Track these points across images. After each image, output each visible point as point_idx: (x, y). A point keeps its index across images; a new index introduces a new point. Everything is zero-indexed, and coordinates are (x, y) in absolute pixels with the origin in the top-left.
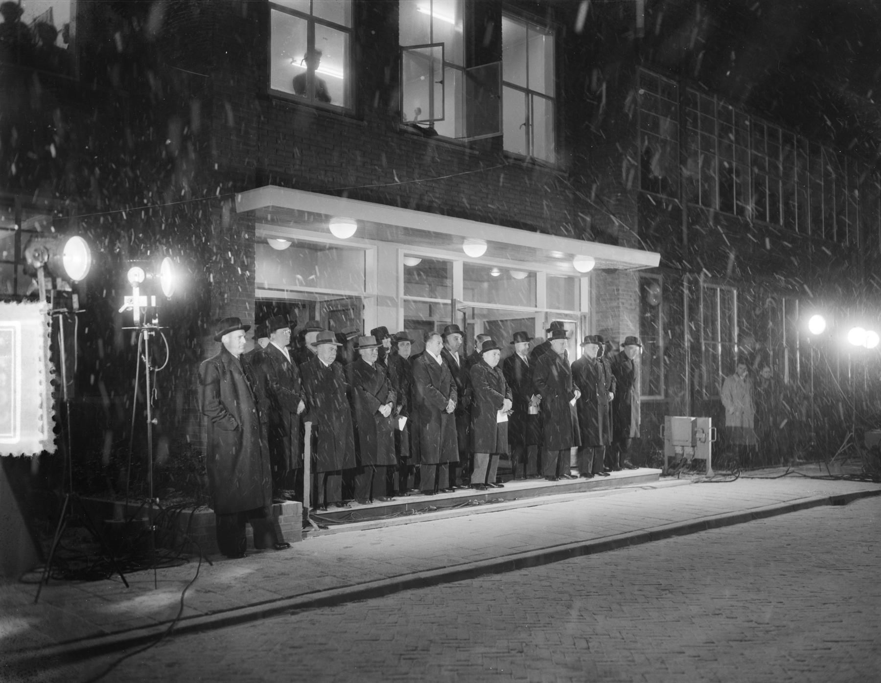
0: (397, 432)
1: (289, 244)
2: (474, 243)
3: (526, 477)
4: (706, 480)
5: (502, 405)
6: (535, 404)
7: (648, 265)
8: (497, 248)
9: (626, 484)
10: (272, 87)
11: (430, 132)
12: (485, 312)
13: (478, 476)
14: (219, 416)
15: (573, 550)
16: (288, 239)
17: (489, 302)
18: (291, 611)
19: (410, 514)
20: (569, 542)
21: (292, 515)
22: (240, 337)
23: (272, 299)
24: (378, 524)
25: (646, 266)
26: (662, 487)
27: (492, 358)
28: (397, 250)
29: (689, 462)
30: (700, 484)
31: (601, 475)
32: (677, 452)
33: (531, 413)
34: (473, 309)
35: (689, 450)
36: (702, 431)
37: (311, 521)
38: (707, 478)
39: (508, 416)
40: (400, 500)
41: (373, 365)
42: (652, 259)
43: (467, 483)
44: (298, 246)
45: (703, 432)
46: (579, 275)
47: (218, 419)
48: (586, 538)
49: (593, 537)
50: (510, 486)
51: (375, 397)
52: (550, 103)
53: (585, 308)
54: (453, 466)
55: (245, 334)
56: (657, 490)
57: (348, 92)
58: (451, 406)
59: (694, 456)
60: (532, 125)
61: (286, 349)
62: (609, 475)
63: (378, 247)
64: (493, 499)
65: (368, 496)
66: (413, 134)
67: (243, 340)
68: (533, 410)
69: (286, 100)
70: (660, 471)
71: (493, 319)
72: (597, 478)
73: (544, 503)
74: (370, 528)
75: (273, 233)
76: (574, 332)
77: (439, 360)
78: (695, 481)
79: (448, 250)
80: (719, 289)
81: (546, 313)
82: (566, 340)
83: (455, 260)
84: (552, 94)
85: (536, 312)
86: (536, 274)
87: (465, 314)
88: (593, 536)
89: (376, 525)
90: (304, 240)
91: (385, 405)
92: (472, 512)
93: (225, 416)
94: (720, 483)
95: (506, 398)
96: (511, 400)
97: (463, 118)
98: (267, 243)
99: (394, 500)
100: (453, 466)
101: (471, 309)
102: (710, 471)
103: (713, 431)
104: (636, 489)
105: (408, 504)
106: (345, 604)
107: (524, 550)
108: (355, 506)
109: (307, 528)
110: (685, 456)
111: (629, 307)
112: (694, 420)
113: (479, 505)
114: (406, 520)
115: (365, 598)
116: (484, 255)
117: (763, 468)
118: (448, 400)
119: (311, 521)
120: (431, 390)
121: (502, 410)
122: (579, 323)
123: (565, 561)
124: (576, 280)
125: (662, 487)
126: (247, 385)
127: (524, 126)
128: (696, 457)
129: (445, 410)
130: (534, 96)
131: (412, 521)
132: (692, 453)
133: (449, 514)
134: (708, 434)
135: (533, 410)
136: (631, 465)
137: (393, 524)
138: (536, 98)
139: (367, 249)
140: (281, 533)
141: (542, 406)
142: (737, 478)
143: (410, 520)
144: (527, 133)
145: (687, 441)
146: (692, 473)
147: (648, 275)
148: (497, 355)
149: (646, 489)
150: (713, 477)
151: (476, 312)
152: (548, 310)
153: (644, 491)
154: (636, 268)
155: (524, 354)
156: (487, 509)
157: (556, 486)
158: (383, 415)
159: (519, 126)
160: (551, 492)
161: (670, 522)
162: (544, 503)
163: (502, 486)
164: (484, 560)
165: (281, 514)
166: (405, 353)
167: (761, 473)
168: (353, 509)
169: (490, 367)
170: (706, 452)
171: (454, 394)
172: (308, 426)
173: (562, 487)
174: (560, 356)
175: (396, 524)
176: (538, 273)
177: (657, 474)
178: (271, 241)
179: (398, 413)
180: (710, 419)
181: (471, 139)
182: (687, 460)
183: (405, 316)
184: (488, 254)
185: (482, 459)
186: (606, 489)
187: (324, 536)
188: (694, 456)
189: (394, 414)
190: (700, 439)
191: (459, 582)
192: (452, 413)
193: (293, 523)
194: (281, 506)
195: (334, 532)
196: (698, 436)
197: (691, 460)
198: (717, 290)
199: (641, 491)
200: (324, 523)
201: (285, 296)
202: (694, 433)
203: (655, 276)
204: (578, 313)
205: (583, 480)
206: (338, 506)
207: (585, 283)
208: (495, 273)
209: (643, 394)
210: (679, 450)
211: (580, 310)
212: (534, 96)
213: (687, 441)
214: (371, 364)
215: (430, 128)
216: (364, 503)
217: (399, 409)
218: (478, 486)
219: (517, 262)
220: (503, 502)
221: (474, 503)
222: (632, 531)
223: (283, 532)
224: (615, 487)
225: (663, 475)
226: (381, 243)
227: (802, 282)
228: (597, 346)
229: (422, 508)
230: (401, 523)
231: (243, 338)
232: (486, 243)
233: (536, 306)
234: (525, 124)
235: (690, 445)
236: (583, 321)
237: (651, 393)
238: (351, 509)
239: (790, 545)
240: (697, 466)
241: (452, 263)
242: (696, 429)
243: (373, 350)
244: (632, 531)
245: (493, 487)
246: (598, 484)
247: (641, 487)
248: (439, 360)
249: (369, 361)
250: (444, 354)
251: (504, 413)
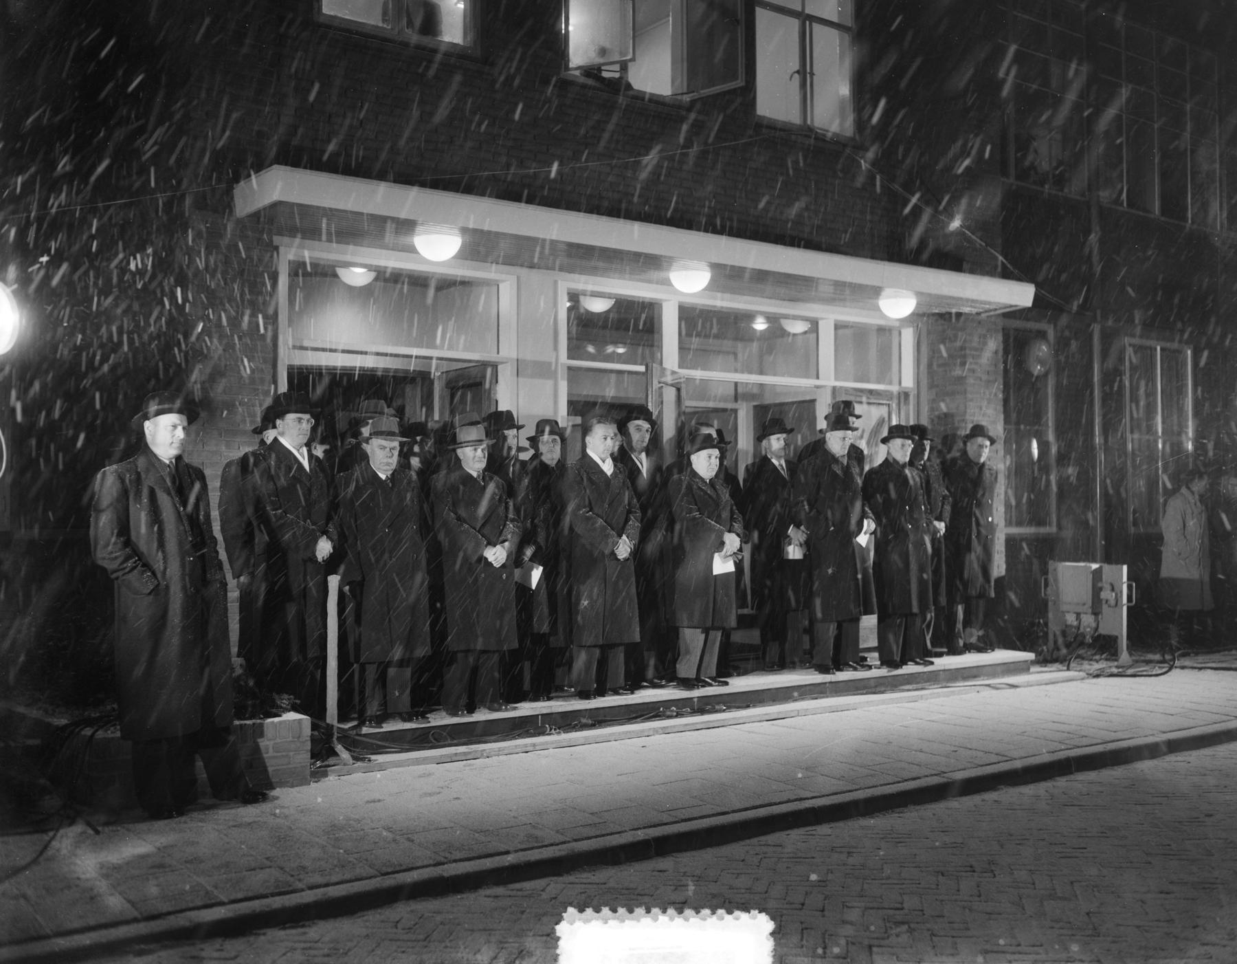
0: (523, 589)
1: (373, 275)
2: (686, 268)
3: (781, 665)
4: (1115, 671)
5: (723, 543)
6: (797, 542)
7: (1013, 303)
8: (727, 277)
9: (965, 678)
10: (325, 10)
11: (619, 86)
12: (755, 391)
13: (686, 668)
14: (124, 569)
15: (812, 811)
16: (369, 268)
17: (761, 373)
18: (137, 947)
19: (543, 733)
20: (785, 799)
21: (291, 739)
22: (175, 427)
23: (353, 369)
24: (470, 753)
25: (1011, 306)
26: (1029, 685)
27: (705, 463)
28: (556, 282)
29: (1089, 640)
30: (1102, 680)
31: (917, 663)
32: (1069, 623)
33: (791, 557)
34: (736, 384)
35: (1088, 620)
36: (1109, 587)
37: (339, 748)
38: (1117, 667)
39: (735, 562)
40: (526, 709)
41: (479, 476)
42: (1021, 295)
43: (668, 676)
44: (388, 279)
45: (1113, 590)
46: (897, 324)
47: (120, 573)
48: (823, 792)
49: (834, 789)
50: (740, 684)
51: (479, 532)
52: (847, 37)
53: (908, 381)
54: (633, 651)
55: (185, 424)
56: (1018, 689)
57: (468, 19)
58: (624, 549)
59: (1096, 629)
60: (812, 74)
61: (609, 462)
62: (932, 663)
63: (518, 278)
64: (704, 706)
65: (464, 701)
66: (594, 88)
67: (180, 433)
68: (794, 552)
69: (385, 40)
70: (1031, 656)
71: (768, 400)
72: (910, 669)
73: (799, 713)
74: (454, 759)
75: (348, 258)
76: (887, 419)
77: (608, 467)
78: (1095, 673)
79: (650, 281)
80: (1159, 348)
81: (834, 388)
82: (850, 432)
83: (666, 300)
84: (849, 22)
85: (817, 387)
86: (817, 323)
87: (679, 390)
88: (842, 786)
89: (465, 754)
90: (411, 271)
91: (495, 546)
93: (133, 568)
94: (1137, 679)
95: (730, 531)
96: (738, 535)
97: (682, 61)
98: (335, 276)
99: (515, 709)
100: (633, 651)
101: (733, 385)
102: (1125, 656)
103: (1130, 587)
104: (978, 688)
105: (542, 715)
106: (262, 931)
107: (687, 816)
108: (440, 719)
109: (330, 759)
110: (1082, 630)
111: (984, 377)
112: (1096, 570)
113: (676, 716)
114: (526, 746)
115: (308, 920)
116: (705, 289)
117: (1230, 650)
118: (620, 536)
119: (339, 748)
120: (588, 519)
121: (723, 553)
122: (894, 405)
123: (763, 839)
124: (895, 333)
125: (1029, 685)
126: (179, 512)
127: (796, 75)
128: (1102, 631)
129: (613, 554)
130: (814, 25)
131: (537, 748)
132: (1094, 625)
133: (610, 735)
134: (1121, 592)
135: (794, 552)
136: (982, 645)
137: (499, 752)
138: (817, 28)
139: (584, 293)
140: (266, 770)
141: (808, 545)
142: (1170, 669)
143: (534, 745)
144: (803, 85)
145: (1084, 604)
146: (1097, 657)
147: (1018, 324)
148: (713, 458)
149: (997, 689)
150: (1130, 667)
151: (740, 390)
152: (838, 384)
153: (994, 692)
154: (996, 310)
155: (779, 458)
156: (686, 725)
157: (831, 683)
158: (491, 564)
159: (788, 77)
160: (822, 693)
161: (1000, 758)
162: (799, 713)
163: (726, 684)
164: (596, 837)
165: (262, 735)
166: (549, 456)
167: (1223, 658)
168: (433, 724)
169: (702, 480)
170: (1118, 624)
171: (634, 524)
172: (334, 581)
173: (808, 688)
174: (840, 459)
175: (506, 752)
176: (820, 323)
177: (1026, 661)
178: (341, 272)
179: (526, 559)
180: (1125, 568)
181: (695, 95)
182: (1084, 637)
183: (569, 395)
184: (713, 286)
185: (692, 638)
186: (922, 689)
187: (360, 774)
188: (1096, 629)
189: (516, 560)
190: (1107, 601)
191: (518, 886)
192: (626, 560)
193: (291, 754)
194: (261, 725)
195: (381, 768)
196: (1103, 595)
197: (1092, 637)
198: (1156, 349)
199: (987, 693)
200: (362, 749)
201: (369, 362)
202: (1097, 591)
203: (1032, 325)
204: (894, 389)
205: (884, 672)
206: (405, 720)
207: (908, 337)
208: (760, 325)
209: (1009, 523)
210: (1071, 619)
211: (900, 383)
212: (814, 25)
213: (1084, 604)
214: (475, 474)
215: (621, 78)
216: (455, 714)
217: (529, 552)
218: (687, 684)
219: (786, 303)
220: (724, 711)
221: (668, 713)
222: (919, 778)
223: (270, 769)
224: (944, 684)
225: (1035, 662)
226: (524, 272)
227: (729, 112)
228: (910, 442)
229: (567, 722)
230: (517, 751)
231: (180, 428)
232: (708, 268)
233: (818, 378)
234: (798, 72)
235: (1090, 611)
236: (902, 400)
237: (1040, 523)
238: (428, 725)
239: (1210, 816)
240: (1105, 646)
241: (661, 306)
242: (1100, 585)
243: (475, 450)
244: (919, 778)
245: (711, 685)
246: (911, 679)
247: (988, 685)
248: (608, 467)
249: (471, 469)
250: (622, 457)
251: (726, 557)
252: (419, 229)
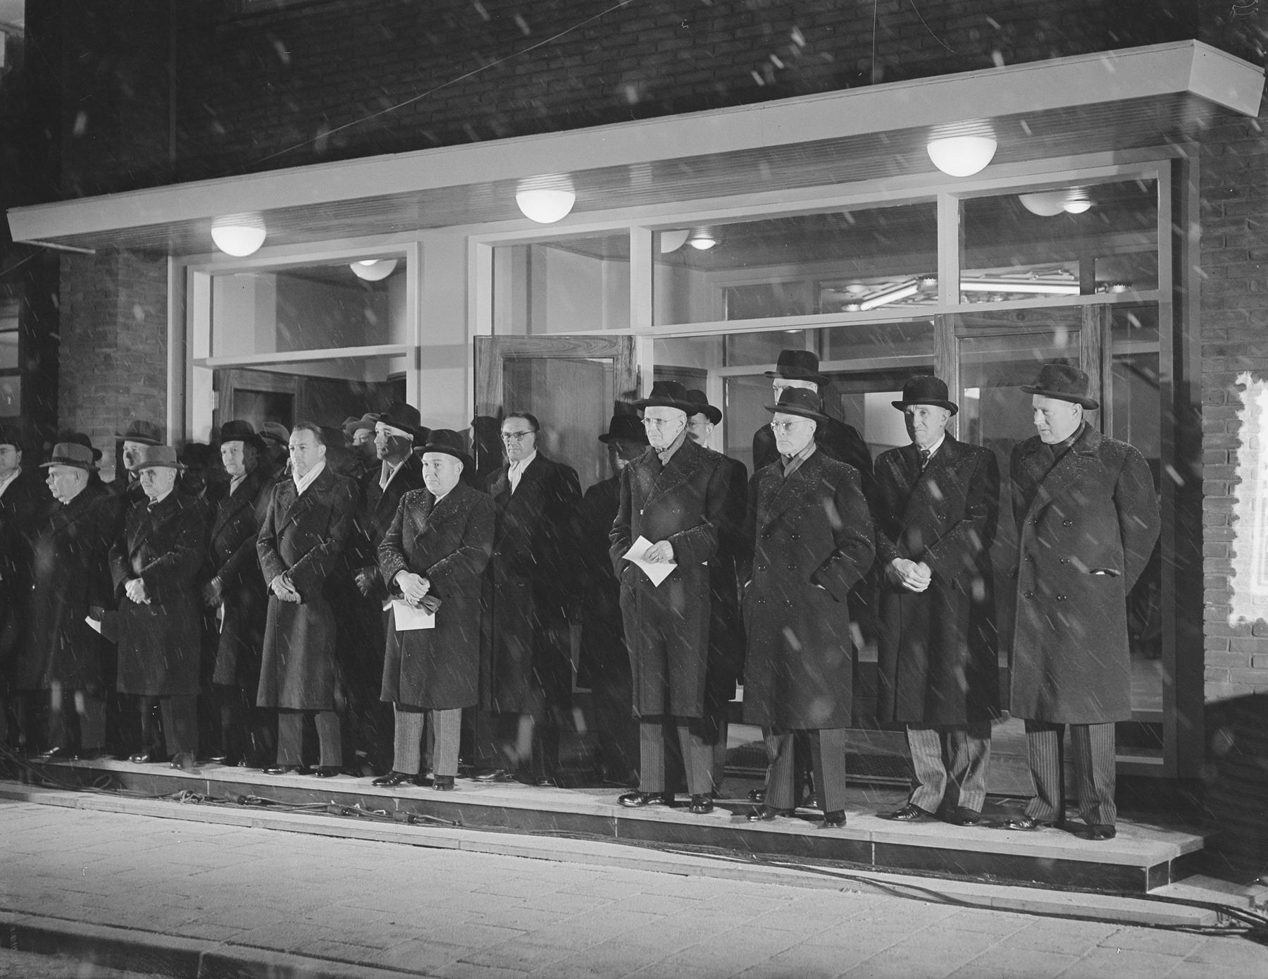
92: (255, 823)
252: (217, 222)
